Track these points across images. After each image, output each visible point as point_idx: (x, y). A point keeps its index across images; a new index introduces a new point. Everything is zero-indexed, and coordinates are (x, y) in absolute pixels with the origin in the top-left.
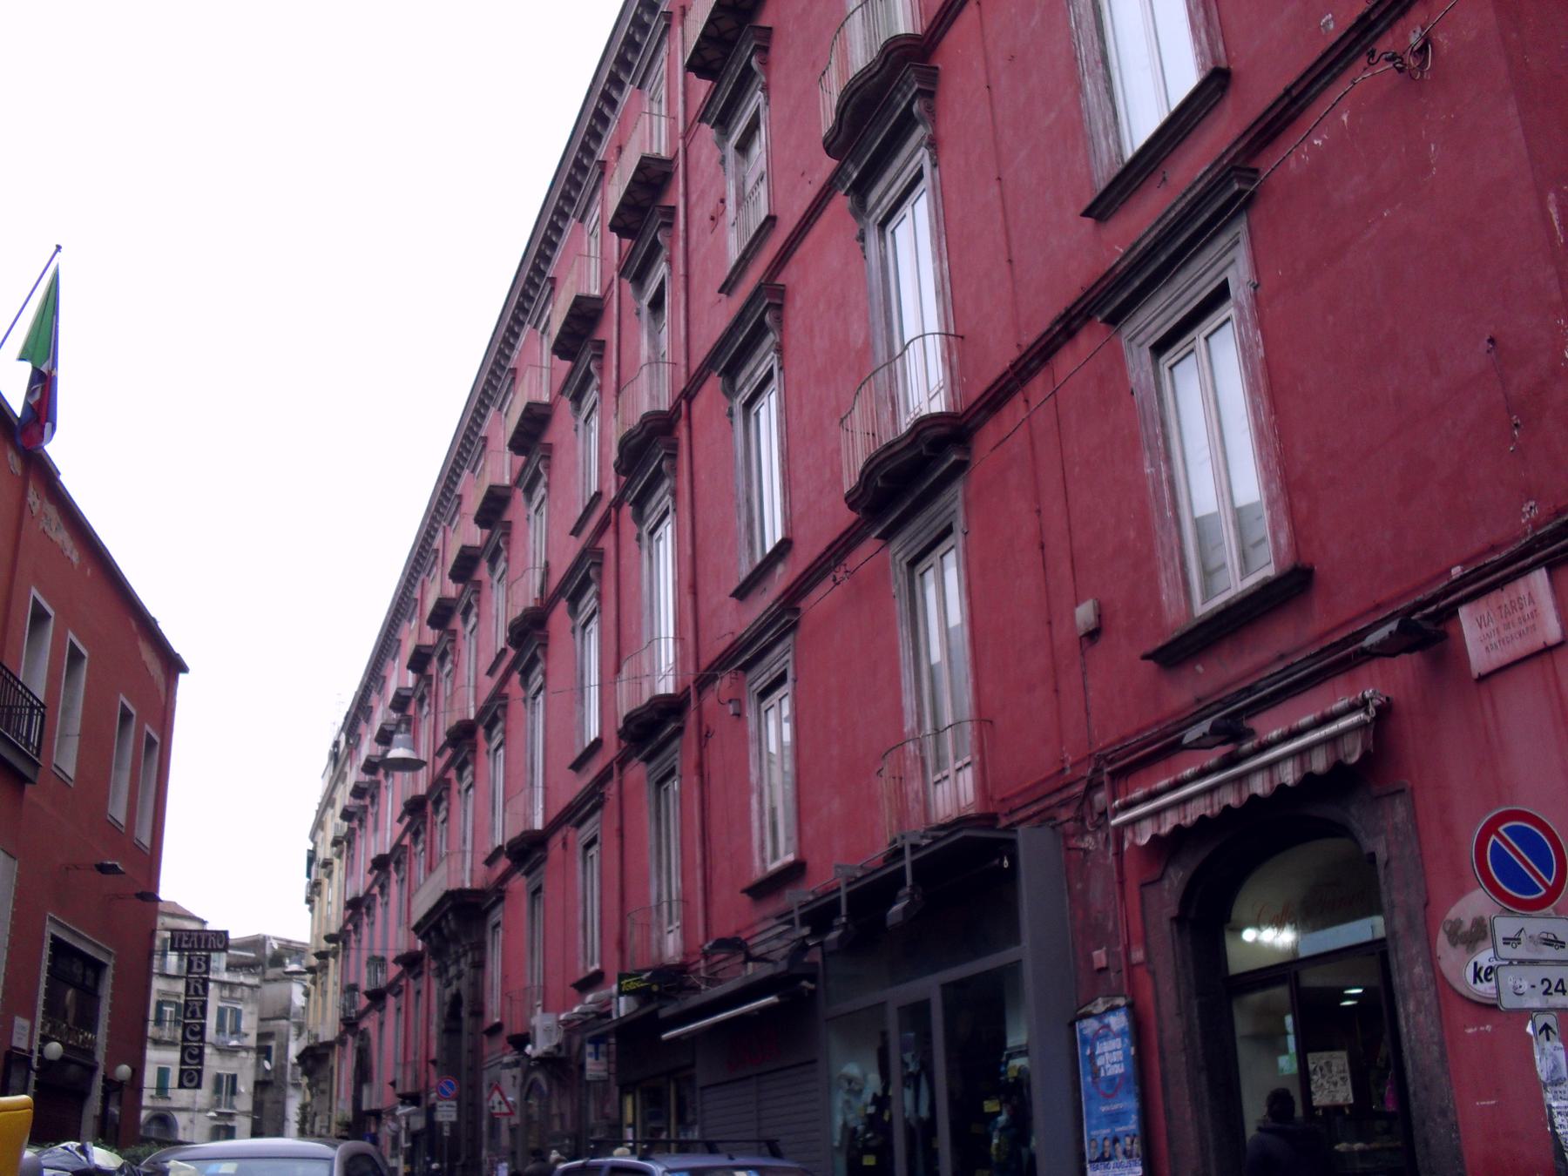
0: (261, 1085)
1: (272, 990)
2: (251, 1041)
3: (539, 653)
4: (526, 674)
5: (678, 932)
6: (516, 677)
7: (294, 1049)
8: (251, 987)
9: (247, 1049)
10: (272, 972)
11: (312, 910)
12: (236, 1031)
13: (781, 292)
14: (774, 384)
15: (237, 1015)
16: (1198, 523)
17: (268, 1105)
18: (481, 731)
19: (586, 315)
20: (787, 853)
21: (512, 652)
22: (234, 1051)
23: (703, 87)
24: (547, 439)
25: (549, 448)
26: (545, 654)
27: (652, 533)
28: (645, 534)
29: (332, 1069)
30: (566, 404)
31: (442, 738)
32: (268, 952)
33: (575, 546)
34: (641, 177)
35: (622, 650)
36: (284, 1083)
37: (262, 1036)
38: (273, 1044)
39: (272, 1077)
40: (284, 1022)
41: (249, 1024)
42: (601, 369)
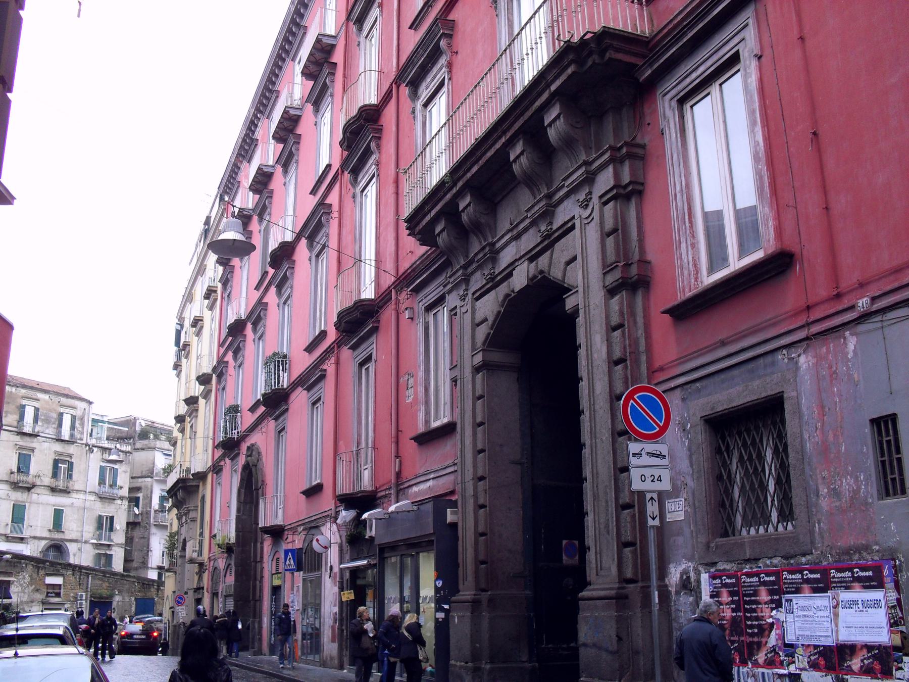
0: (132, 525)
1: (139, 456)
2: (125, 492)
3: (373, 145)
4: (280, 287)
5: (370, 468)
6: (273, 289)
7: (157, 492)
8: (125, 452)
9: (122, 498)
10: (139, 444)
11: (178, 375)
12: (113, 485)
13: (452, 25)
14: (445, 89)
15: (115, 473)
16: (706, 215)
17: (136, 540)
18: (249, 326)
19: (323, 52)
20: (444, 417)
21: (271, 271)
22: (112, 499)
23: (207, 301)
24: (271, 187)
25: (272, 192)
26: (378, 146)
27: (362, 191)
28: (358, 195)
29: (203, 497)
30: (279, 169)
31: (225, 331)
32: (138, 429)
33: (313, 201)
34: (312, 59)
35: (346, 262)
36: (149, 524)
37: (131, 490)
38: (140, 495)
39: (140, 519)
40: (149, 479)
41: (123, 480)
42: (333, 81)
